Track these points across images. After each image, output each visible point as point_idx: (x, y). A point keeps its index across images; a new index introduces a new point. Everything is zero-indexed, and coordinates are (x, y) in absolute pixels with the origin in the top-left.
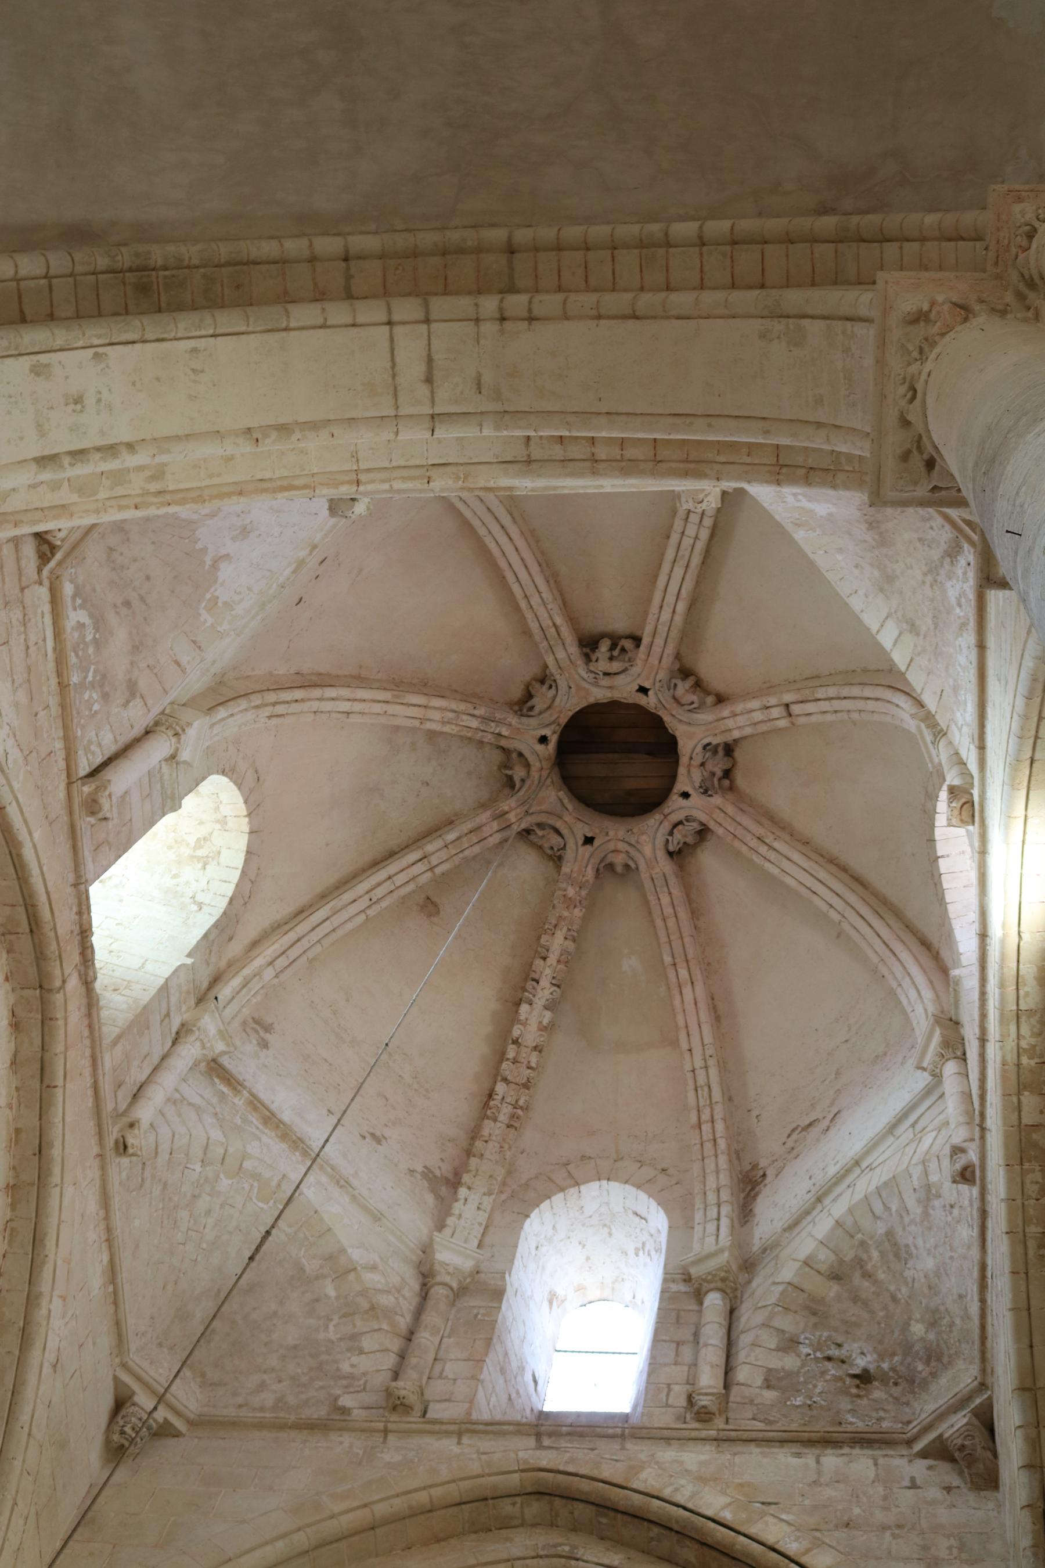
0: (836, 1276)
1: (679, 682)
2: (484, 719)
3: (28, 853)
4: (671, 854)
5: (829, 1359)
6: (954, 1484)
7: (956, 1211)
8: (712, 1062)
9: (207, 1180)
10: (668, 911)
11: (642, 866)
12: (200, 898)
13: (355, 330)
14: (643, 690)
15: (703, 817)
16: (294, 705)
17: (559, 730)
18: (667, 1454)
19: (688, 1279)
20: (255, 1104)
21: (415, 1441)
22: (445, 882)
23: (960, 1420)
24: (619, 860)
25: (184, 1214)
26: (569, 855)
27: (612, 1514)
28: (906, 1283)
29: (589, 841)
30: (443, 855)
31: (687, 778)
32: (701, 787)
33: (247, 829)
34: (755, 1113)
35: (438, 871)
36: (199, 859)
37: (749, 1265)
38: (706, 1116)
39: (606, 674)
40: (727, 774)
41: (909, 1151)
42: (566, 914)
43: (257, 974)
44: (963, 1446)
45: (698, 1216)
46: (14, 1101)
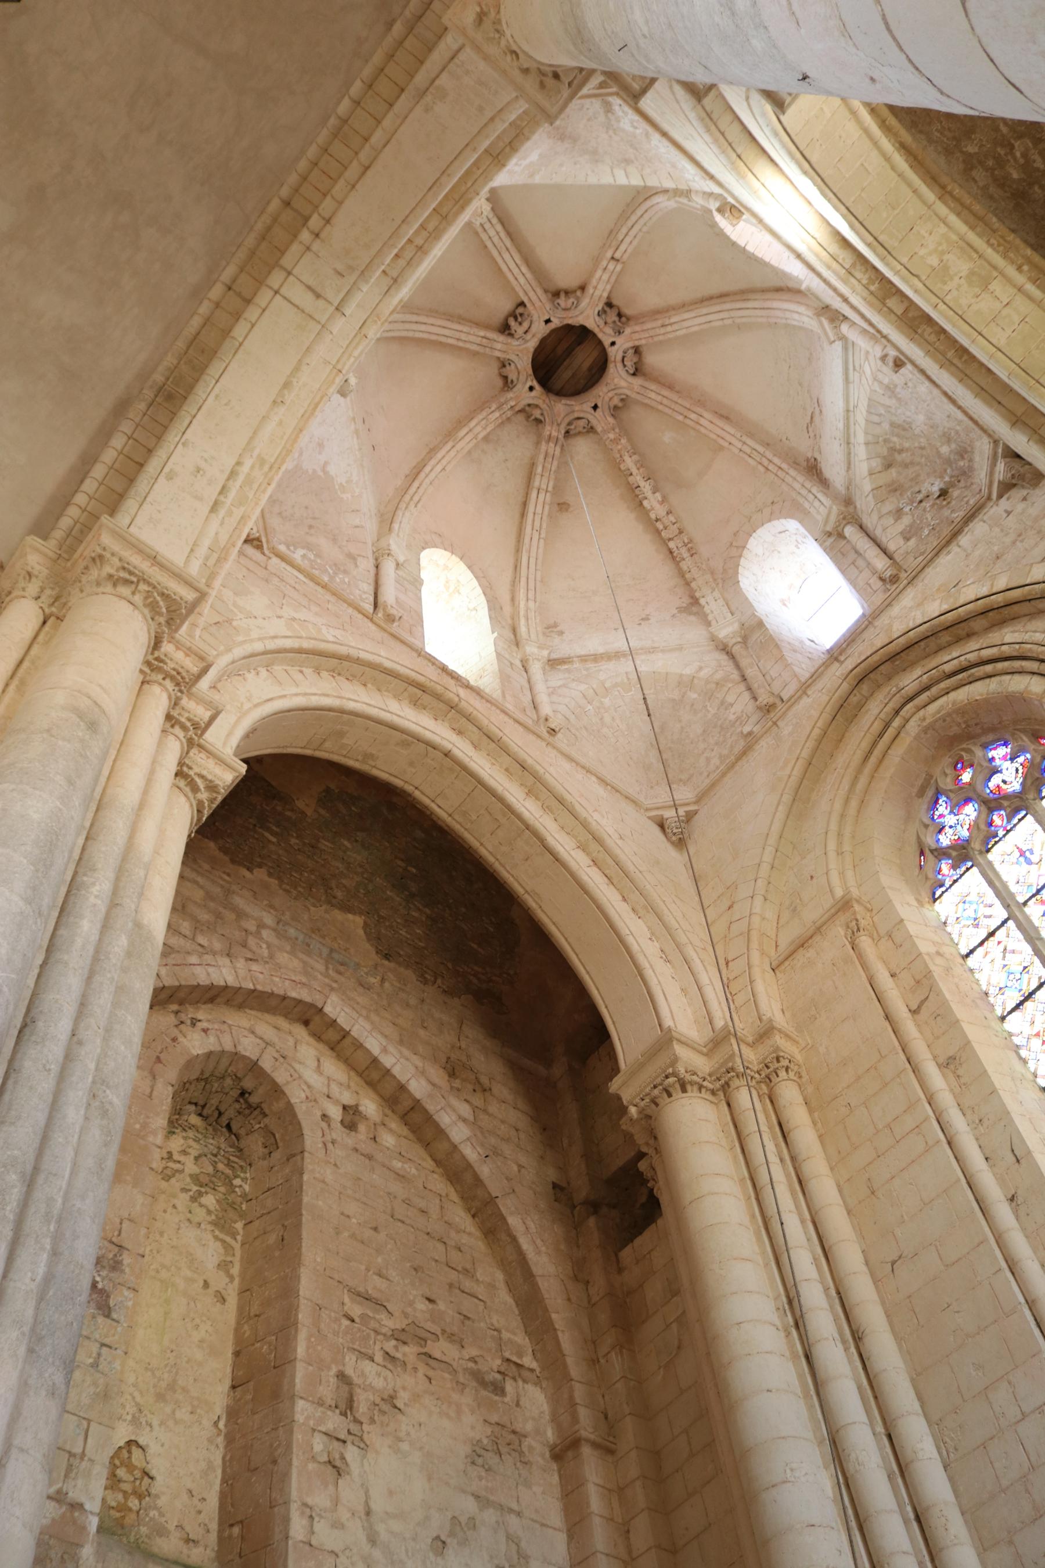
0: (888, 466)
1: (559, 301)
2: (499, 408)
4: (634, 374)
5: (921, 501)
7: (910, 384)
10: (659, 398)
11: (628, 392)
14: (548, 321)
15: (630, 344)
17: (533, 377)
18: (896, 610)
20: (583, 659)
21: (790, 714)
22: (558, 490)
23: (1001, 466)
24: (616, 401)
26: (594, 422)
29: (595, 407)
30: (545, 480)
35: (550, 489)
37: (848, 502)
38: (766, 463)
41: (864, 381)
42: (619, 447)
43: (527, 609)
45: (807, 505)
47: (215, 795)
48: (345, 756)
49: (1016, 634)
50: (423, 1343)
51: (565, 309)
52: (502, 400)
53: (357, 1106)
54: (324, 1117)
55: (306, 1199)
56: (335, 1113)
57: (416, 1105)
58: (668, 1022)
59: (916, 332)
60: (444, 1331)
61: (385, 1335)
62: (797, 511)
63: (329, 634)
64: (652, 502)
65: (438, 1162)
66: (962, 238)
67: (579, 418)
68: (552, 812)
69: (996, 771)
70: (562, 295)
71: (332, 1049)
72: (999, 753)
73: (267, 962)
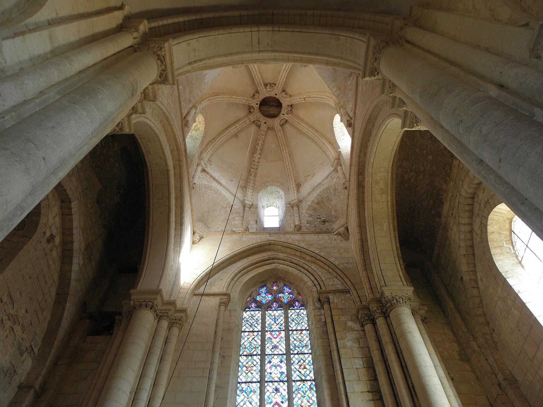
0: (318, 203)
1: (283, 93)
2: (246, 100)
3: (177, 136)
4: (281, 125)
5: (318, 218)
6: (342, 239)
7: (341, 193)
8: (290, 164)
9: (205, 191)
10: (280, 136)
12: (197, 137)
13: (244, 33)
14: (276, 94)
15: (287, 119)
16: (213, 100)
17: (260, 102)
18: (293, 236)
19: (290, 204)
20: (211, 176)
22: (239, 132)
23: (343, 229)
24: (271, 126)
25: (202, 198)
26: (262, 126)
27: (284, 247)
28: (331, 205)
29: (265, 123)
30: (239, 126)
31: (284, 111)
32: (286, 113)
33: (204, 124)
34: (298, 173)
36: (195, 130)
37: (301, 201)
38: (289, 174)
39: (269, 91)
40: (291, 110)
41: (331, 182)
42: (262, 137)
43: (209, 152)
44: (344, 233)
45: (290, 192)
46: (175, 182)
47: (120, 132)
48: (144, 147)
49: (315, 268)
50: (14, 323)
51: (282, 96)
52: (249, 100)
53: (55, 236)
54: (44, 233)
55: (20, 253)
56: (48, 234)
57: (71, 250)
58: (161, 287)
59: (359, 188)
60: (22, 324)
61: (6, 313)
62: (287, 191)
63: (173, 116)
64: (257, 156)
65: (61, 271)
66: (387, 180)
67: (259, 121)
68: (177, 208)
69: (284, 293)
70: (285, 93)
71: (62, 215)
72: (287, 289)
73: (69, 176)
